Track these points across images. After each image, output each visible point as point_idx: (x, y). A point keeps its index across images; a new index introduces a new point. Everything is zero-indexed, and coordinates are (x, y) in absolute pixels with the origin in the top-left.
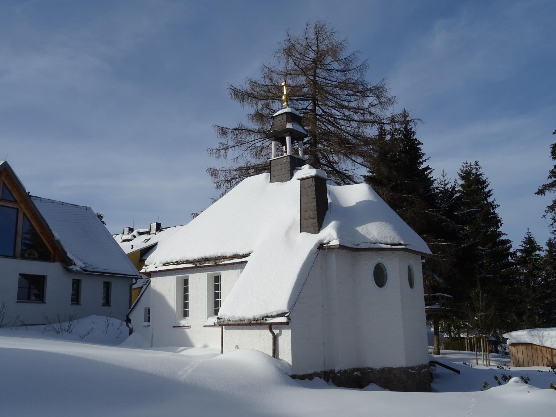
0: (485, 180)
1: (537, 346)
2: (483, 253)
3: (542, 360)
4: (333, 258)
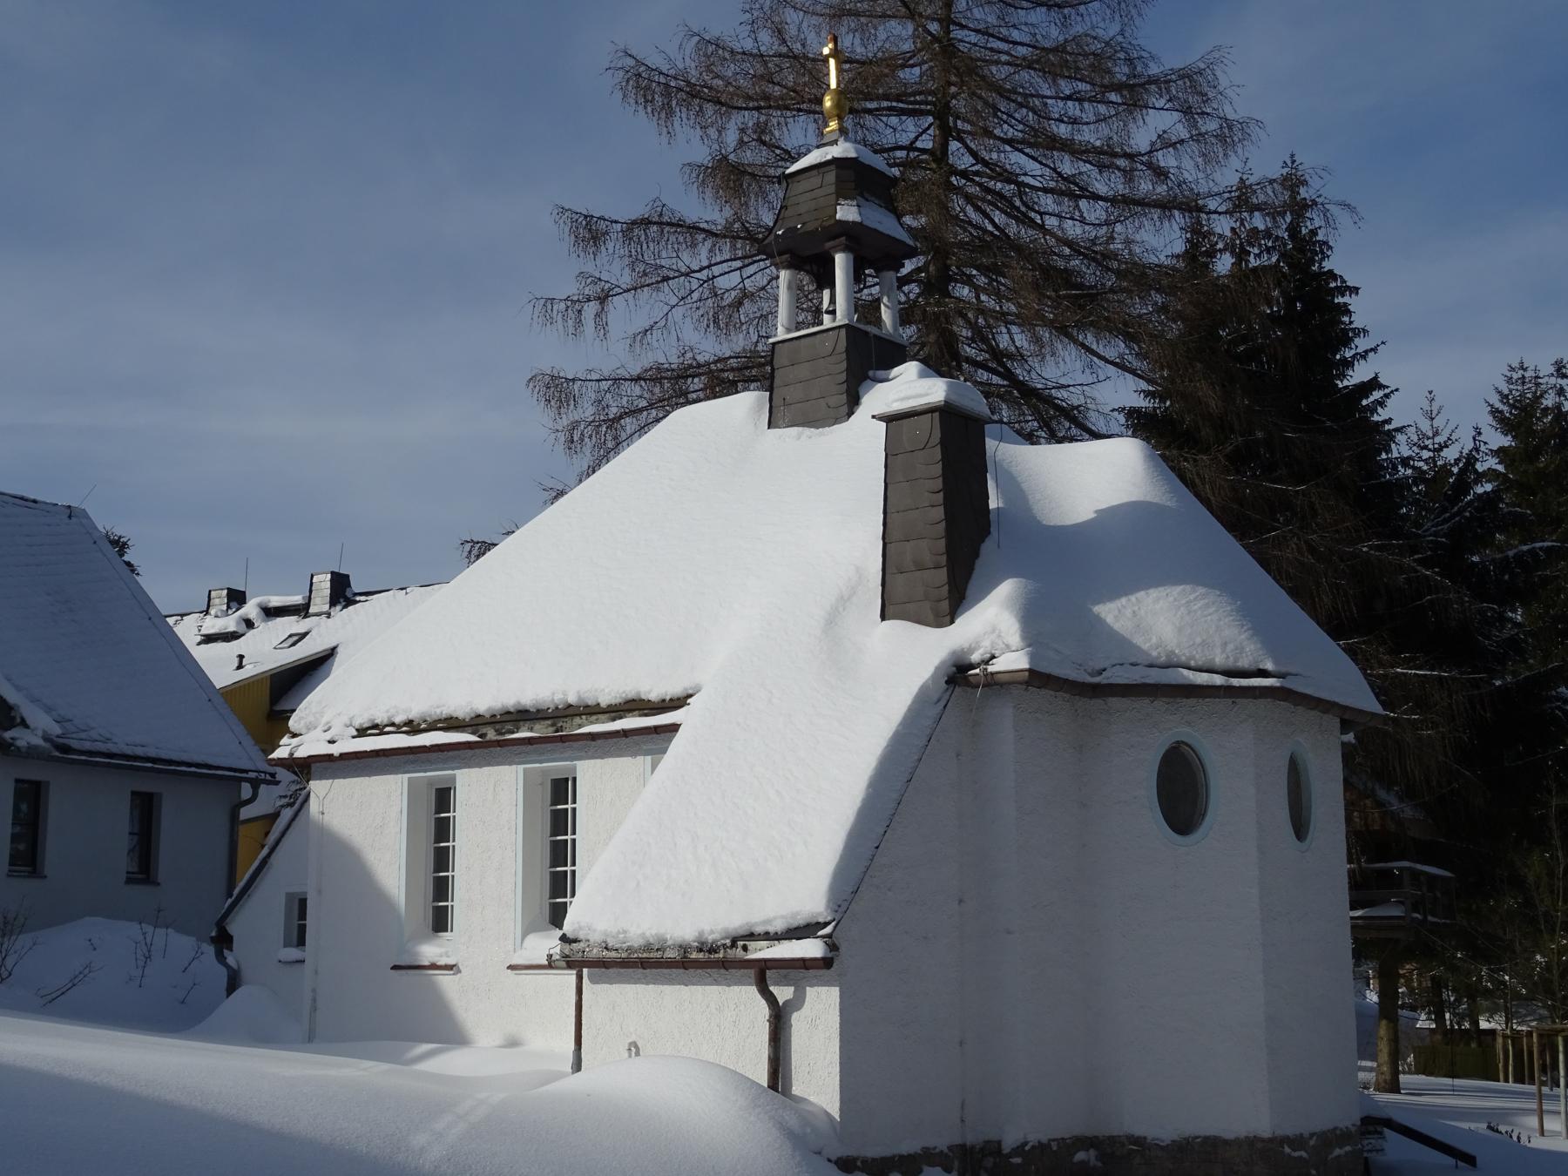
4: (1004, 718)
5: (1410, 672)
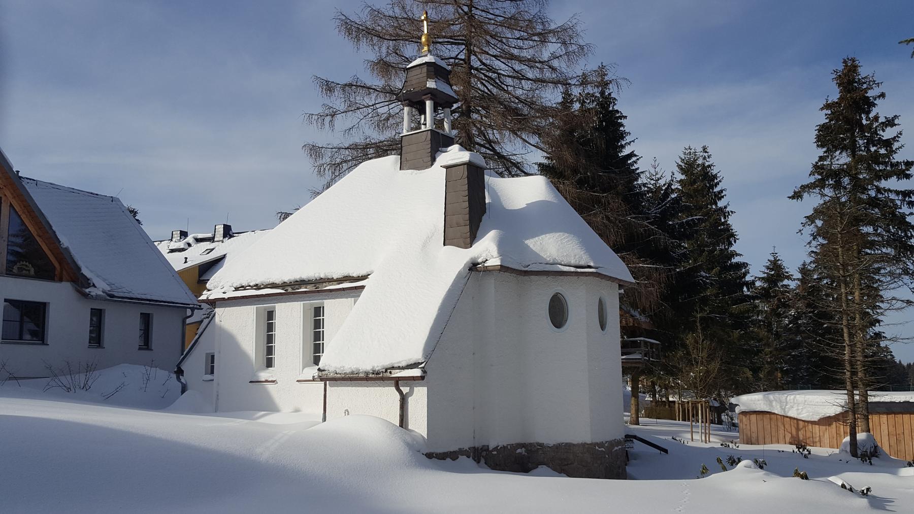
0: (716, 174)
2: (708, 281)
4: (491, 283)
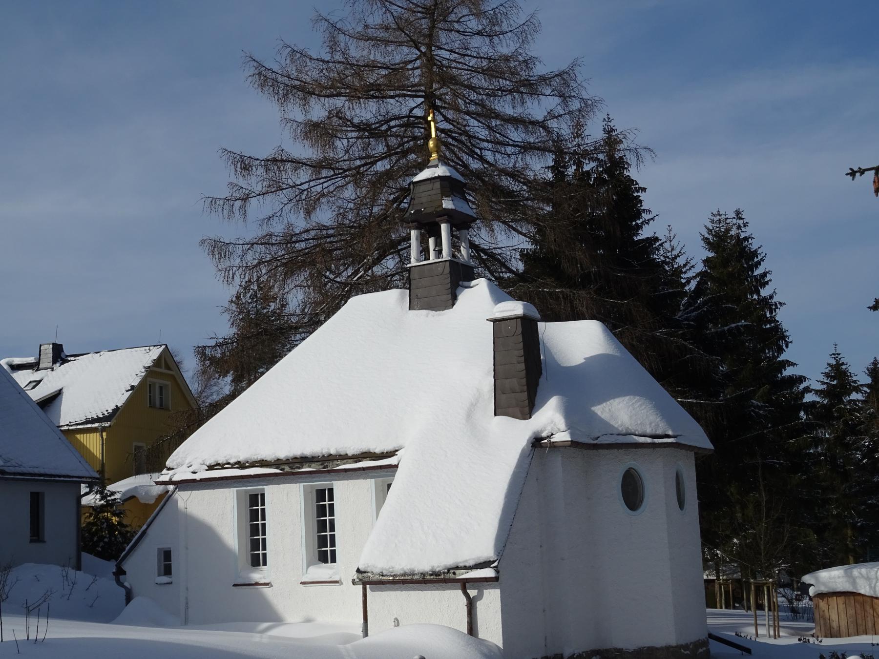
0: (756, 251)
1: (864, 598)
2: (761, 412)
3: (873, 622)
4: (557, 462)
5: (685, 400)
